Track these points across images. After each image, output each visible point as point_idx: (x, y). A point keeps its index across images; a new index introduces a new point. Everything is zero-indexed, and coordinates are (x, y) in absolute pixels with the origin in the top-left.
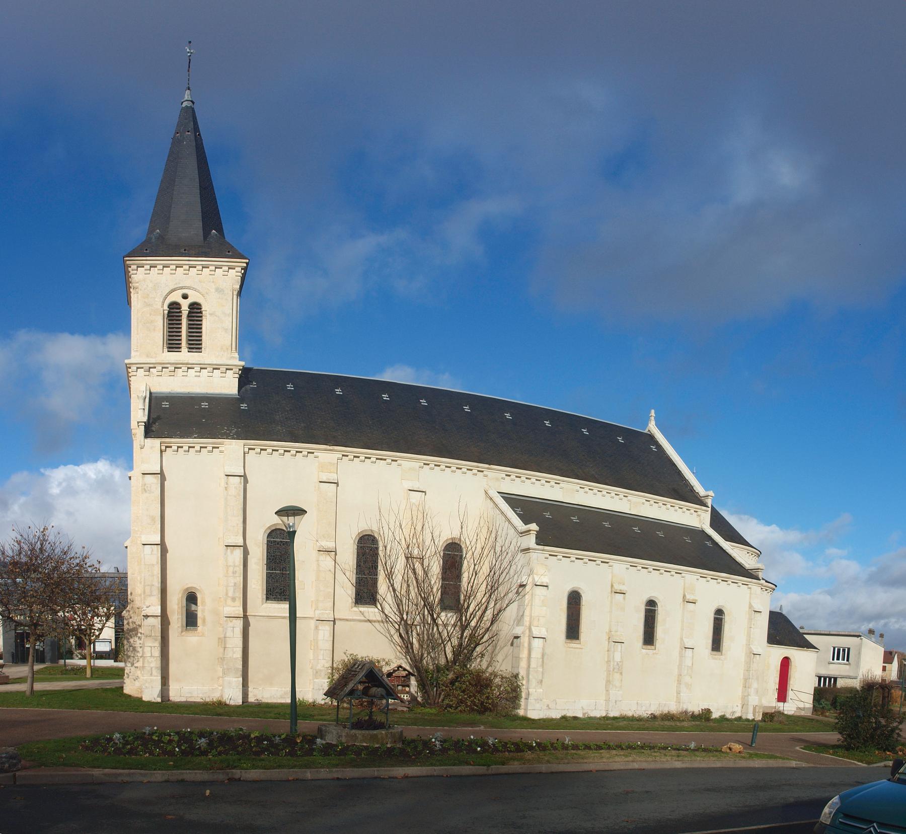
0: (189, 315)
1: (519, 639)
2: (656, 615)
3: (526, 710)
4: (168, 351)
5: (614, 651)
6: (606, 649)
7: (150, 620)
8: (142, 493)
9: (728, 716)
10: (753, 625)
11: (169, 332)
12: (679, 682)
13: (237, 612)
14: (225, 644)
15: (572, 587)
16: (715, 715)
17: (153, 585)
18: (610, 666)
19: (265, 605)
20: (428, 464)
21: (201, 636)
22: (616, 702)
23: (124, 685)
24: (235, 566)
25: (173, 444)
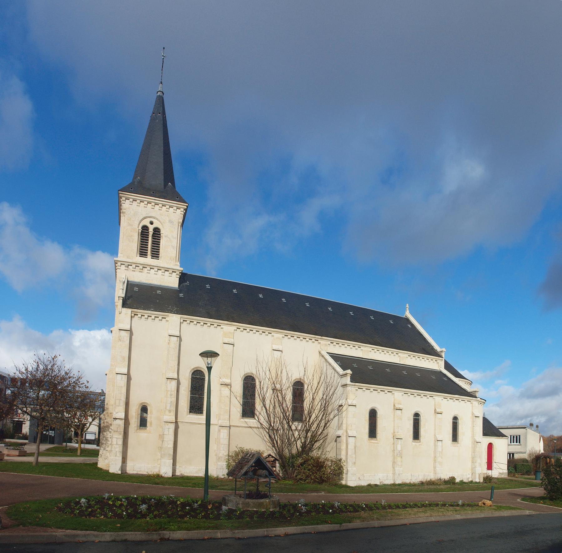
0: (153, 235)
1: (340, 438)
2: (420, 421)
3: (346, 480)
4: (140, 256)
5: (397, 444)
6: (392, 443)
7: (118, 421)
8: (118, 342)
9: (465, 481)
10: (475, 425)
11: (141, 244)
12: (435, 461)
13: (171, 419)
14: (163, 439)
15: (372, 406)
16: (457, 480)
17: (121, 399)
18: (395, 453)
19: (189, 416)
20: (287, 336)
21: (149, 433)
22: (399, 475)
23: (98, 462)
24: (171, 391)
25: (139, 313)
